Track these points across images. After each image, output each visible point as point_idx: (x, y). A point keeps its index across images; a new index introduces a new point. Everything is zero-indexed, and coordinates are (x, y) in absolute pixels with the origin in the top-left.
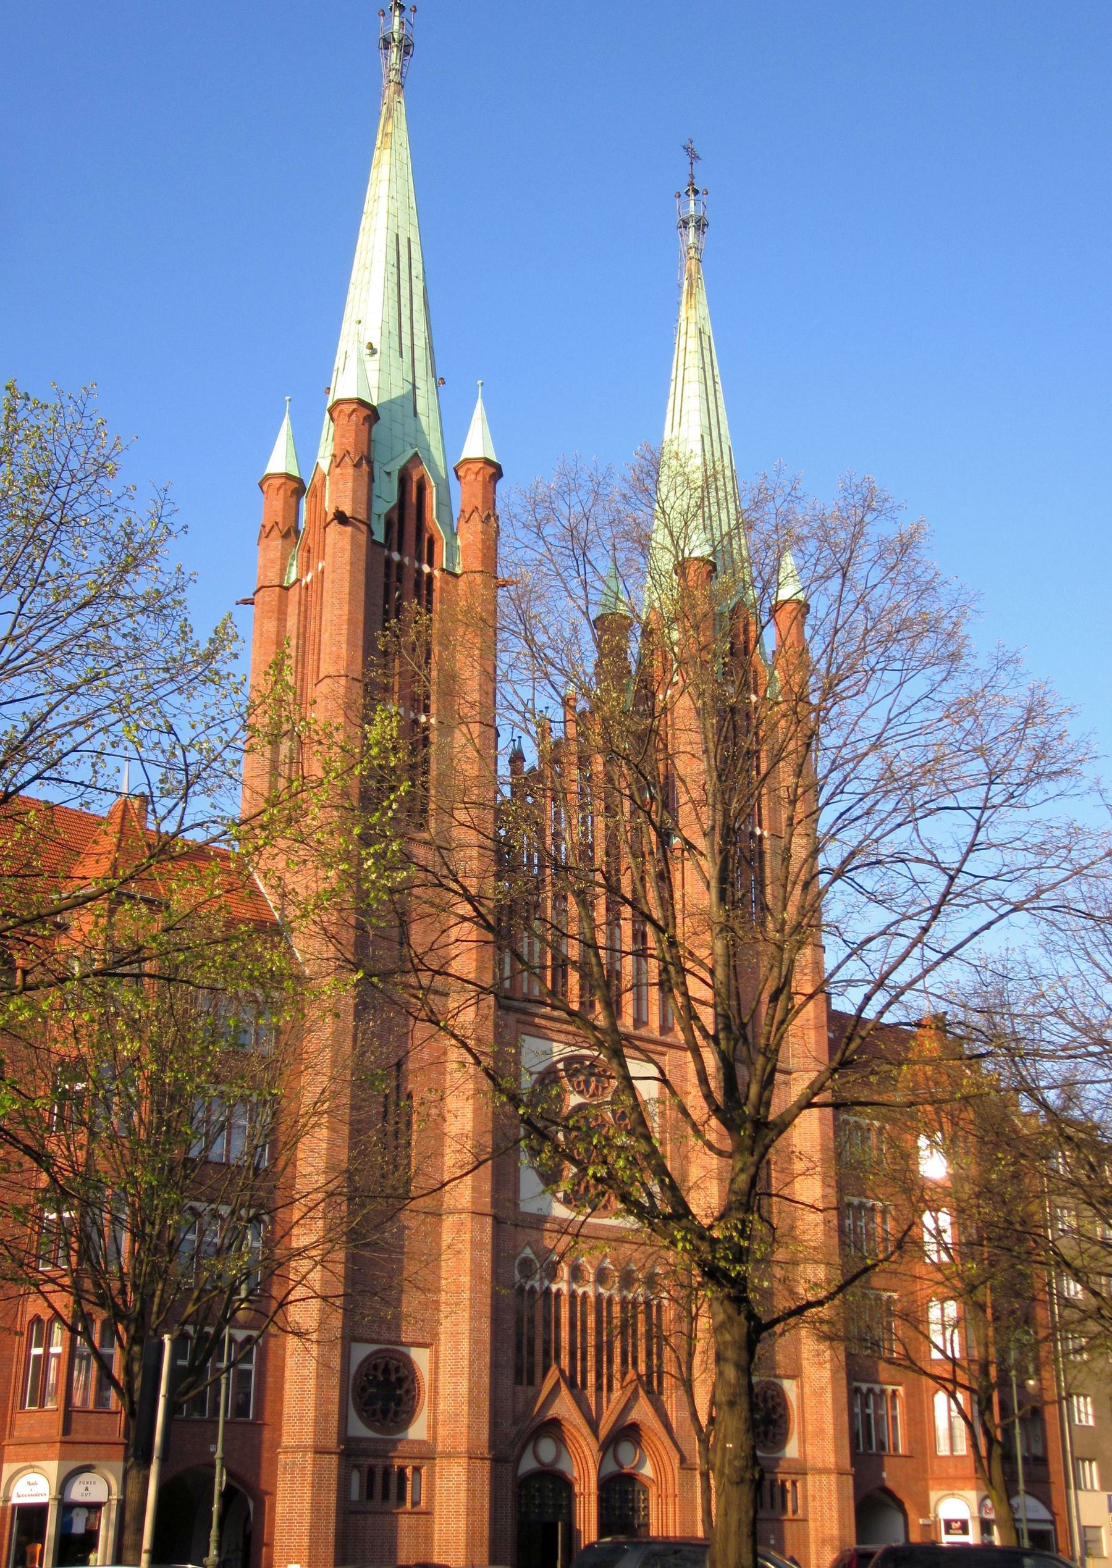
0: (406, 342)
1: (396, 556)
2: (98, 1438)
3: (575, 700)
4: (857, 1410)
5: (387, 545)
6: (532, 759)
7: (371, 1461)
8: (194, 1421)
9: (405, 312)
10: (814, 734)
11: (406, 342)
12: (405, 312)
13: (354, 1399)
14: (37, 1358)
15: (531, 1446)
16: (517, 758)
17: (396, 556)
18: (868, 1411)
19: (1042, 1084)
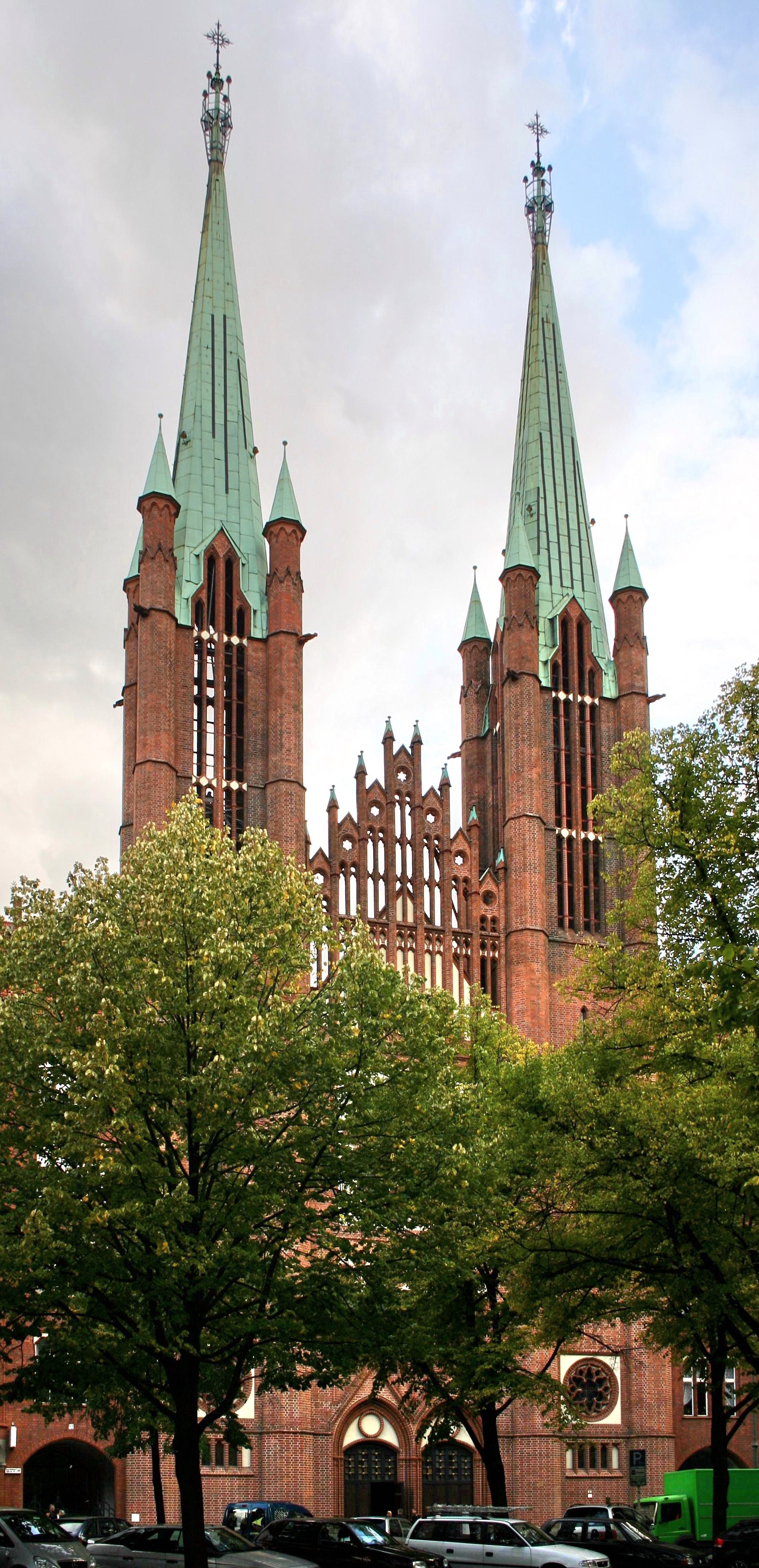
0: (219, 420)
9: (219, 390)
11: (219, 420)
12: (219, 390)
13: (616, 1382)
17: (562, 696)
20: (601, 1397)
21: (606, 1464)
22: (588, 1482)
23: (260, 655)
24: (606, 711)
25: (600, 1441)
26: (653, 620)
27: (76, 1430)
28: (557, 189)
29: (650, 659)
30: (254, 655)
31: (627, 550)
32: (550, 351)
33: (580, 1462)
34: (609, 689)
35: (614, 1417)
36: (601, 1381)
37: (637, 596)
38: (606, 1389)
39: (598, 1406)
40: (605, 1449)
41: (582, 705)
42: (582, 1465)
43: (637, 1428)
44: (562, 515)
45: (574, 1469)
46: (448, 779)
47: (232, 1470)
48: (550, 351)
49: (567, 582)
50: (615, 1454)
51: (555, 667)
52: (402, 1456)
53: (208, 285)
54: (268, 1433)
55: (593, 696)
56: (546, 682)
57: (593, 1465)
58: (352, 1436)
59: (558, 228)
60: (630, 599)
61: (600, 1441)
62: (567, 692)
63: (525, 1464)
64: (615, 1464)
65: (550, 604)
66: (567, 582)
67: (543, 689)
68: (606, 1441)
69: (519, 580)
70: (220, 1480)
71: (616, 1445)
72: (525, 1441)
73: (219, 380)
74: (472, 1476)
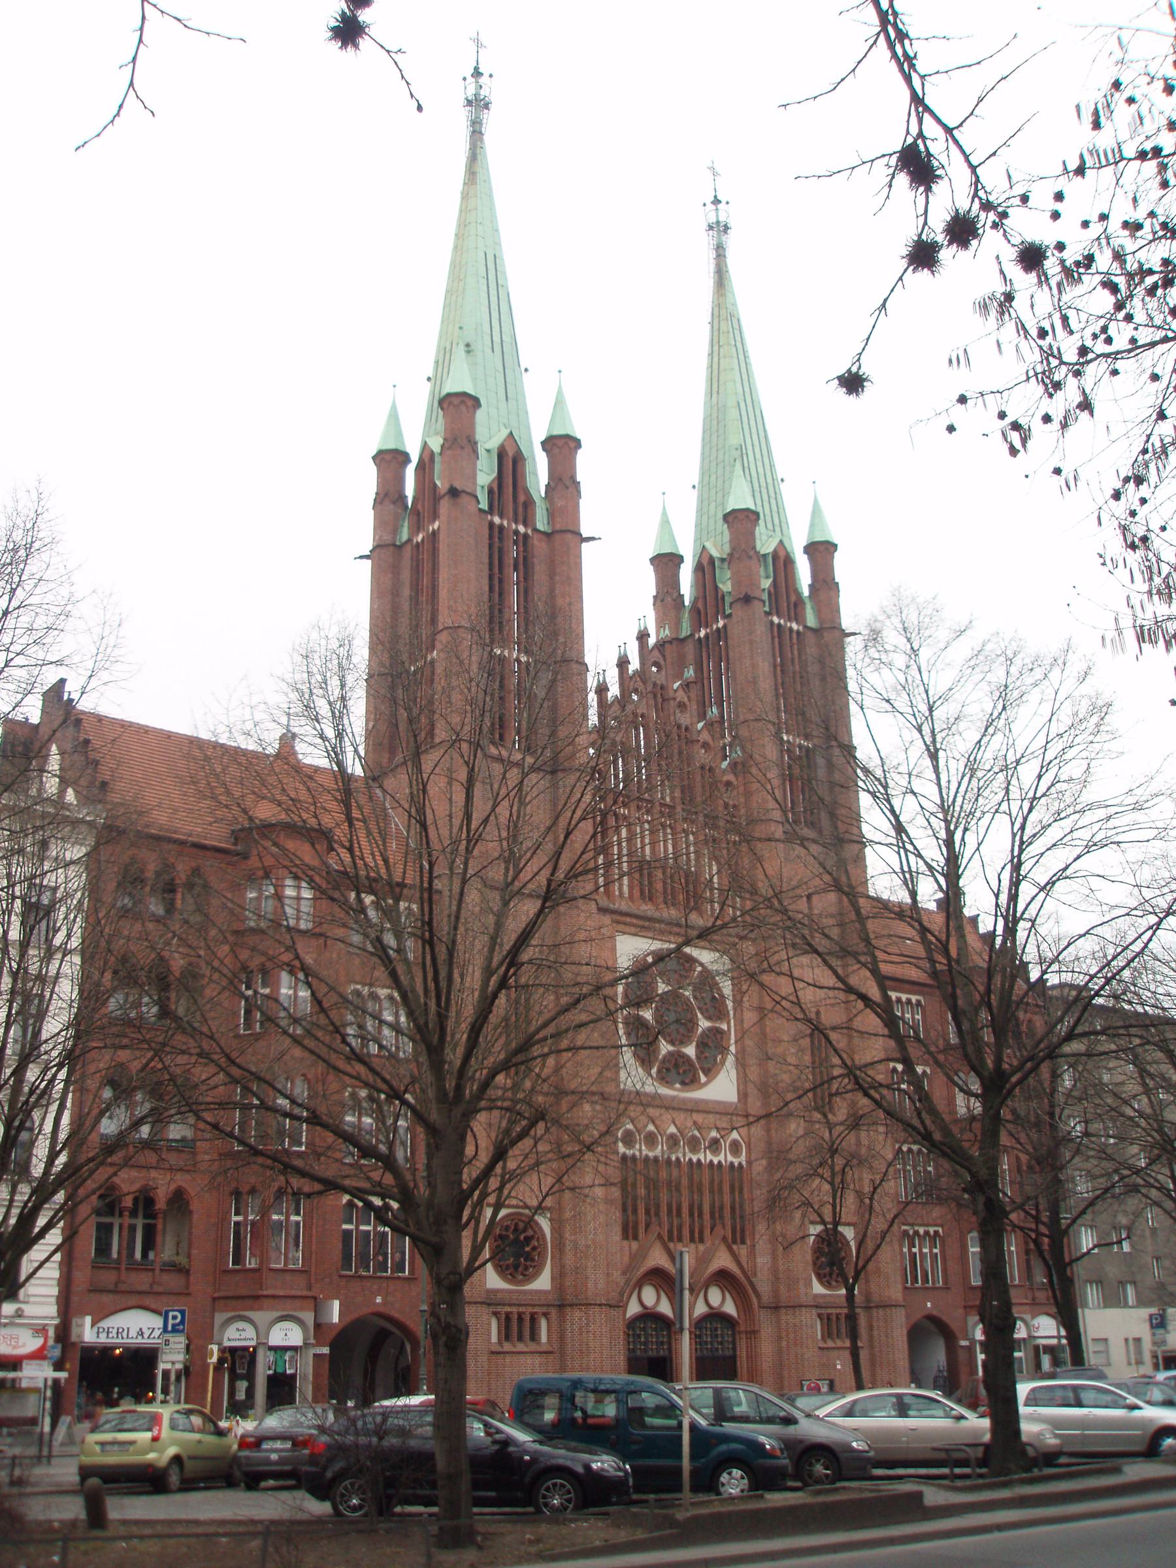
0: (497, 339)
1: (497, 520)
2: (293, 1293)
3: (929, 1329)
4: (905, 1250)
5: (491, 511)
6: (614, 690)
7: (508, 1309)
8: (361, 1277)
9: (495, 315)
10: (851, 1071)
11: (497, 339)
12: (495, 315)
13: (544, 1235)
14: (237, 1224)
15: (635, 1296)
16: (602, 689)
17: (497, 520)
18: (915, 1250)
19: (863, 1134)
20: (529, 1257)
21: (534, 1336)
22: (836, 1352)
23: (544, 545)
24: (811, 639)
25: (530, 1309)
26: (585, 466)
27: (384, 1303)
28: (491, 89)
29: (583, 504)
30: (539, 547)
31: (816, 511)
32: (738, 338)
33: (506, 1335)
34: (811, 620)
35: (543, 1282)
36: (528, 1240)
37: (572, 445)
38: (534, 1248)
39: (526, 1268)
40: (533, 1319)
41: (791, 629)
42: (830, 1335)
43: (875, 1298)
44: (761, 470)
45: (500, 1342)
46: (626, 656)
47: (533, 1347)
48: (738, 338)
49: (770, 526)
50: (544, 1324)
51: (491, 492)
52: (742, 1328)
53: (480, 228)
54: (571, 1305)
55: (525, 525)
56: (484, 505)
57: (520, 1338)
58: (633, 1309)
59: (492, 122)
60: (562, 447)
61: (530, 1309)
62: (501, 517)
63: (792, 1336)
64: (544, 1338)
65: (489, 434)
66: (770, 526)
67: (481, 510)
68: (536, 1310)
69: (457, 408)
70: (521, 1357)
71: (545, 1315)
72: (790, 1311)
73: (494, 306)
74: (734, 1349)
